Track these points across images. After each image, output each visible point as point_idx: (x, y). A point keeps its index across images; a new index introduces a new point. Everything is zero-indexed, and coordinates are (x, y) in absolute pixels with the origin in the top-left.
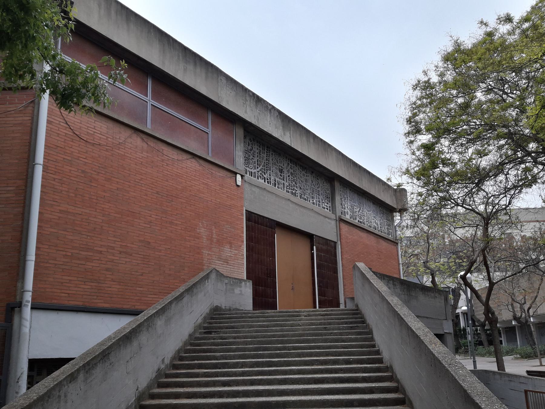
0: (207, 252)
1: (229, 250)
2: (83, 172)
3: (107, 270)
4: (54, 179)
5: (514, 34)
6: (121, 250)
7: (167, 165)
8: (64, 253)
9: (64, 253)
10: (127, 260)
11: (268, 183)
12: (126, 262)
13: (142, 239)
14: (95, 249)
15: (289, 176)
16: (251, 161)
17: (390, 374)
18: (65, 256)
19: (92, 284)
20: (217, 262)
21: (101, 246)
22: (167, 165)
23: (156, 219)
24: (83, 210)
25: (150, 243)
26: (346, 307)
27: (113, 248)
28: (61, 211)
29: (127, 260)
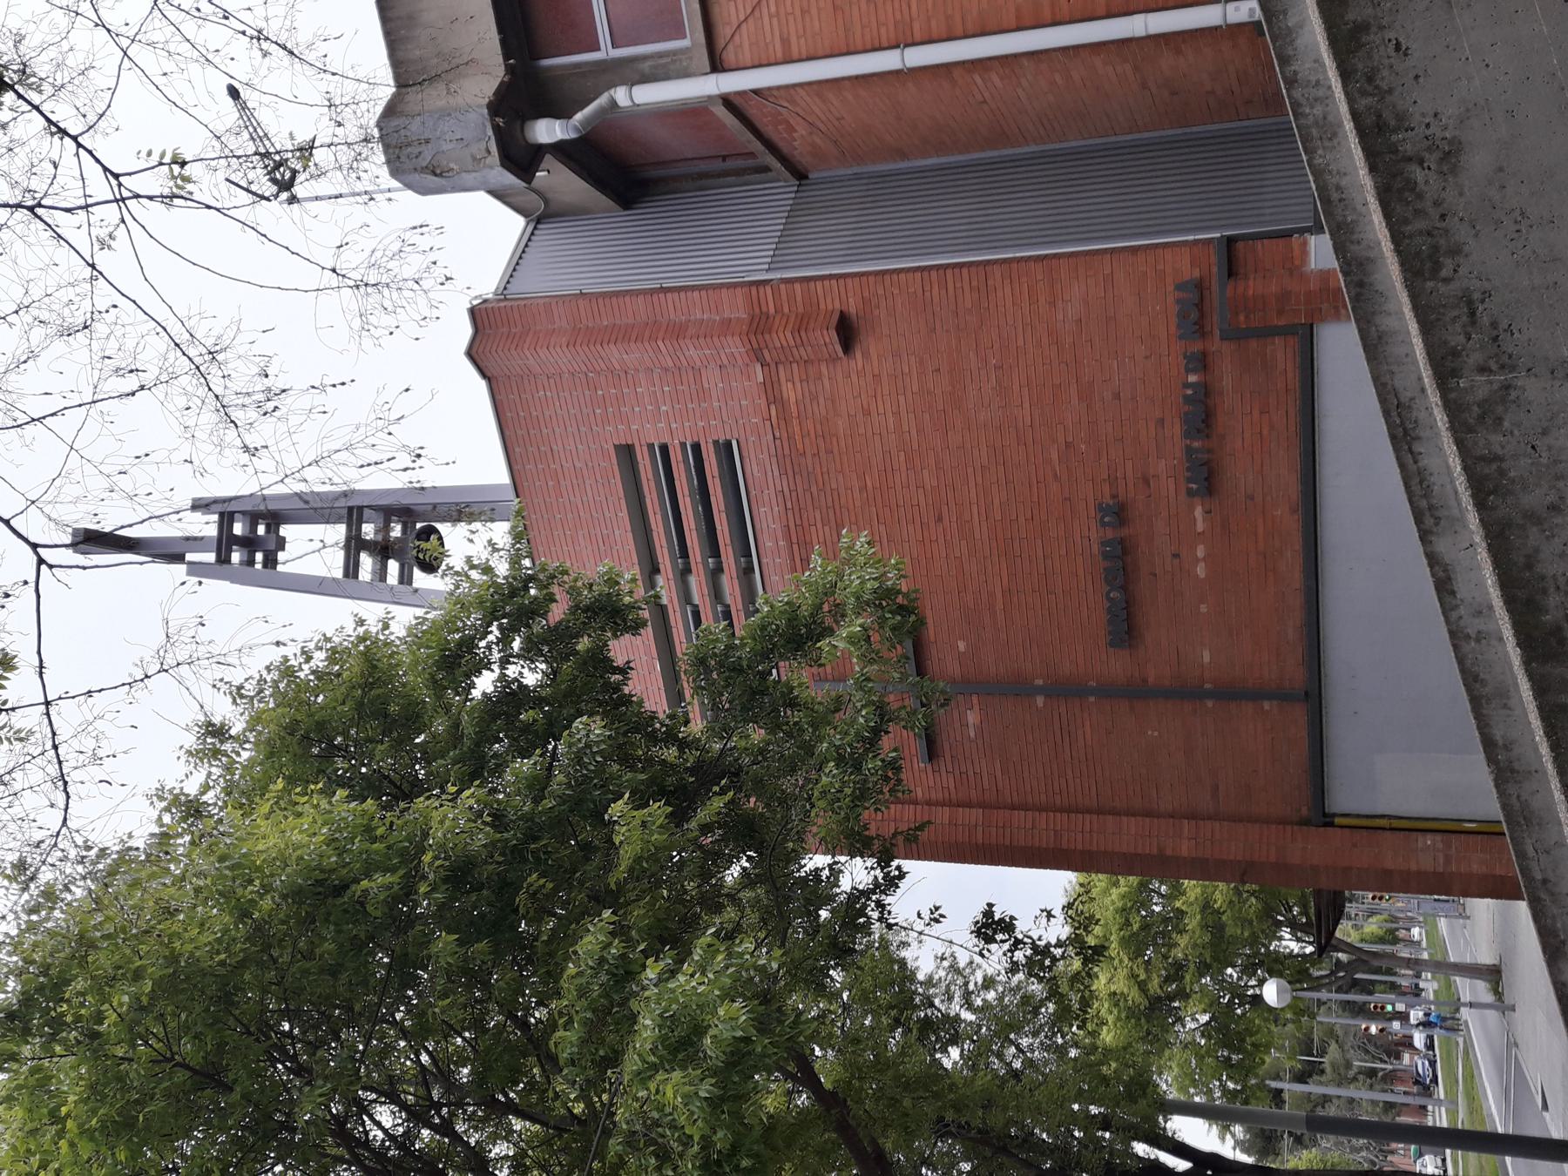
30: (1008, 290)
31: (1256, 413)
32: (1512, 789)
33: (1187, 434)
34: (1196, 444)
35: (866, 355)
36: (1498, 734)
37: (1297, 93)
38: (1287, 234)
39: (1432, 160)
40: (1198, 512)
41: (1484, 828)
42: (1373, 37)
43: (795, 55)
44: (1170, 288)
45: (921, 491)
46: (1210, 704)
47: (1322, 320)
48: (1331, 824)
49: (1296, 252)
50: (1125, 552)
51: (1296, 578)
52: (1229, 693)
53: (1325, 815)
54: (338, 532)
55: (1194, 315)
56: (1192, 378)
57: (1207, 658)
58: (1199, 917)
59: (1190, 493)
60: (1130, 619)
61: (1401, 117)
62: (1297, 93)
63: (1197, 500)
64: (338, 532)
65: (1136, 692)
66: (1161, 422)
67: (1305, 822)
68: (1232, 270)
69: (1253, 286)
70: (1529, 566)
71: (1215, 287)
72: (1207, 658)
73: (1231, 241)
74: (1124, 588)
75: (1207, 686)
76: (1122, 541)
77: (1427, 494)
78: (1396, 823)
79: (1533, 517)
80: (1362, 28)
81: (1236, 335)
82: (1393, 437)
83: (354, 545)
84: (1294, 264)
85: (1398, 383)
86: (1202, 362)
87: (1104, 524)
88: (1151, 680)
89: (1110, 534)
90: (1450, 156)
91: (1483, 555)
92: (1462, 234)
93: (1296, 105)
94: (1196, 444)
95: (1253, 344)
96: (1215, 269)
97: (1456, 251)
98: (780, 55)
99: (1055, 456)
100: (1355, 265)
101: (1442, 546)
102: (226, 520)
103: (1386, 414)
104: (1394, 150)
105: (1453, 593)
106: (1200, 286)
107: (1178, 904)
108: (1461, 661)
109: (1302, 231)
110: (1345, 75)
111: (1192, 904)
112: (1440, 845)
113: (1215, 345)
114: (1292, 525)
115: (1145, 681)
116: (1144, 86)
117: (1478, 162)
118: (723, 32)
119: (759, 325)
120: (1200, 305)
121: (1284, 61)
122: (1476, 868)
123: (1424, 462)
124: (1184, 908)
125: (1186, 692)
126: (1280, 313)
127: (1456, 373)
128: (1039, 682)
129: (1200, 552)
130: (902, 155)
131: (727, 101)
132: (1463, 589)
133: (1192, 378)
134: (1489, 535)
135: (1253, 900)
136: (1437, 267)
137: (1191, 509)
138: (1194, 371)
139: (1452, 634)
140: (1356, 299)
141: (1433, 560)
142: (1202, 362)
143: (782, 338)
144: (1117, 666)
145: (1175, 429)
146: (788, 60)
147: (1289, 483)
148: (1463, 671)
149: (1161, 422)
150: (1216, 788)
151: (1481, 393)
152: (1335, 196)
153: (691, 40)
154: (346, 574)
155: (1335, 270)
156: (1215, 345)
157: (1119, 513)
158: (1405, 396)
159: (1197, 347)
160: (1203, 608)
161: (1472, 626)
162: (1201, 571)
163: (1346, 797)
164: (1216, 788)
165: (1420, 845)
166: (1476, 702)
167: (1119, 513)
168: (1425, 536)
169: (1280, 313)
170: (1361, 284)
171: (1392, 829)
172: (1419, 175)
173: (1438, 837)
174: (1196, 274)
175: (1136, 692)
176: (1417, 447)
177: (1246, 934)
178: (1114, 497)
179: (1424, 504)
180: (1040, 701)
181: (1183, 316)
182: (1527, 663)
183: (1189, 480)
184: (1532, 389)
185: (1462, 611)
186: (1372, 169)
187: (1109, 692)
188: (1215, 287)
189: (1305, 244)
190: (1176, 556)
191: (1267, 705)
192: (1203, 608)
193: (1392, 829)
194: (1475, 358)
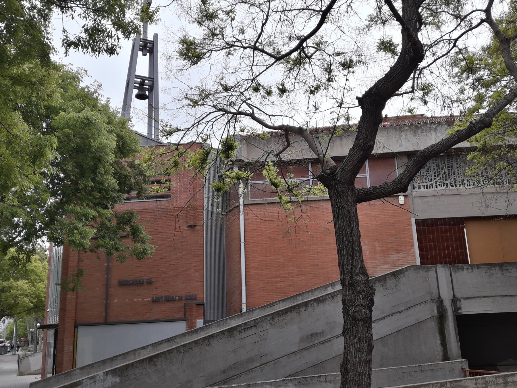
0: (371, 261)
1: (397, 255)
2: (269, 237)
3: (290, 286)
4: (253, 246)
5: (425, 17)
6: (298, 273)
7: (327, 213)
8: (263, 282)
9: (263, 282)
10: (303, 278)
11: (452, 186)
12: (302, 279)
13: (313, 264)
14: (281, 276)
15: (486, 169)
16: (426, 177)
17: (244, 310)
18: (263, 283)
19: (281, 295)
20: (382, 266)
21: (285, 273)
22: (327, 213)
23: (322, 249)
24: (271, 257)
25: (318, 265)
26: (123, 284)
27: (292, 273)
28: (259, 261)
29: (303, 278)
30: (198, 261)
31: (169, 310)
32: (109, 360)
33: (166, 297)
34: (163, 298)
35: (187, 230)
36: (119, 358)
37: (225, 320)
38: (204, 315)
39: (208, 343)
40: (149, 299)
41: (74, 360)
42: (223, 335)
43: (245, 221)
44: (195, 293)
45: (156, 240)
46: (105, 302)
47: (187, 323)
48: (75, 328)
49: (200, 317)
50: (141, 284)
51: (133, 319)
52: (107, 306)
53: (77, 326)
54: (146, 75)
55: (190, 298)
56: (177, 298)
57: (115, 301)
58: (7, 286)
59: (153, 298)
60: (126, 285)
61: (213, 339)
62: (225, 320)
63: (151, 299)
64: (146, 75)
65: (107, 286)
66: (169, 291)
67: (75, 322)
68: (198, 305)
69: (194, 309)
70: (160, 357)
71: (196, 302)
72: (115, 301)
73: (204, 305)
74: (132, 284)
75: (109, 301)
76: (143, 283)
77: (159, 344)
78: (75, 342)
79: (166, 356)
80: (224, 334)
81: (185, 306)
82: (168, 339)
83: (143, 79)
84: (198, 317)
85: (177, 339)
86: (180, 300)
87: (147, 279)
88: (110, 289)
89: (145, 281)
90: (209, 345)
91: (161, 351)
92: (199, 347)
93: (223, 320)
94: (163, 298)
95: (183, 309)
96: (198, 302)
97: (197, 346)
98: (246, 218)
99: (162, 269)
100: (197, 331)
101: (150, 347)
102: (152, 43)
103: (172, 337)
104: (210, 338)
105: (142, 349)
106: (195, 299)
107: (11, 280)
108: (131, 351)
109: (204, 318)
110: (219, 332)
111: (11, 283)
112: (70, 351)
113: (184, 302)
114: (145, 318)
115: (110, 288)
116: (234, 287)
117: (208, 348)
118: (251, 207)
119: (194, 208)
120: (191, 299)
121: (230, 318)
122: (65, 358)
123: (164, 343)
124: (10, 281)
125: (107, 297)
126: (189, 315)
127: (183, 347)
128: (110, 264)
129: (140, 300)
130: (227, 237)
131: (239, 206)
132: (143, 351)
133: (177, 298)
134: (164, 352)
135: (13, 301)
136: (196, 344)
137: (149, 298)
138: (179, 298)
139: (135, 350)
140: (191, 331)
141: (148, 346)
142: (180, 300)
143: (192, 213)
144: (114, 282)
145: (167, 294)
146: (245, 220)
147: (153, 318)
148: (129, 352)
149: (169, 291)
150: (83, 303)
151: (181, 350)
152: (208, 327)
153: (251, 201)
154: (136, 75)
155: (196, 326)
156: (184, 302)
157: (150, 283)
158: (175, 340)
159: (183, 299)
160: (127, 300)
161: (137, 353)
162: (136, 300)
163: (82, 331)
164: (83, 303)
165: (70, 347)
166: (124, 354)
167: (150, 283)
168: (152, 344)
169: (189, 315)
170: (194, 332)
171: (74, 341)
172: (207, 341)
173: (72, 350)
174: (198, 298)
175: (107, 286)
176: (166, 342)
177: (3, 299)
178: (153, 282)
179: (157, 344)
180: (106, 264)
181: (190, 296)
182: (149, 357)
183: (156, 297)
184: (181, 356)
185: (139, 351)
186: (208, 336)
187: (108, 280)
188: (196, 302)
189: (202, 319)
190: (139, 295)
191: (104, 314)
192: (127, 300)
193: (74, 341)
194: (185, 349)
